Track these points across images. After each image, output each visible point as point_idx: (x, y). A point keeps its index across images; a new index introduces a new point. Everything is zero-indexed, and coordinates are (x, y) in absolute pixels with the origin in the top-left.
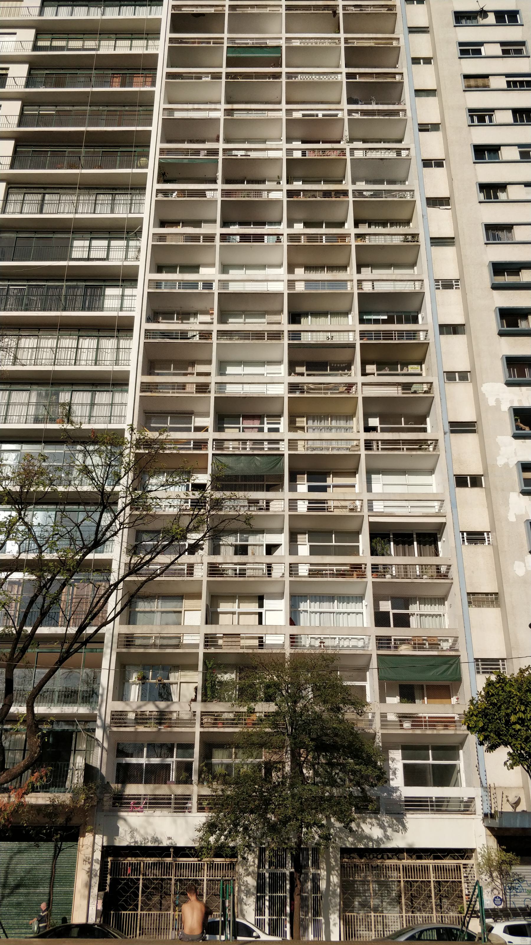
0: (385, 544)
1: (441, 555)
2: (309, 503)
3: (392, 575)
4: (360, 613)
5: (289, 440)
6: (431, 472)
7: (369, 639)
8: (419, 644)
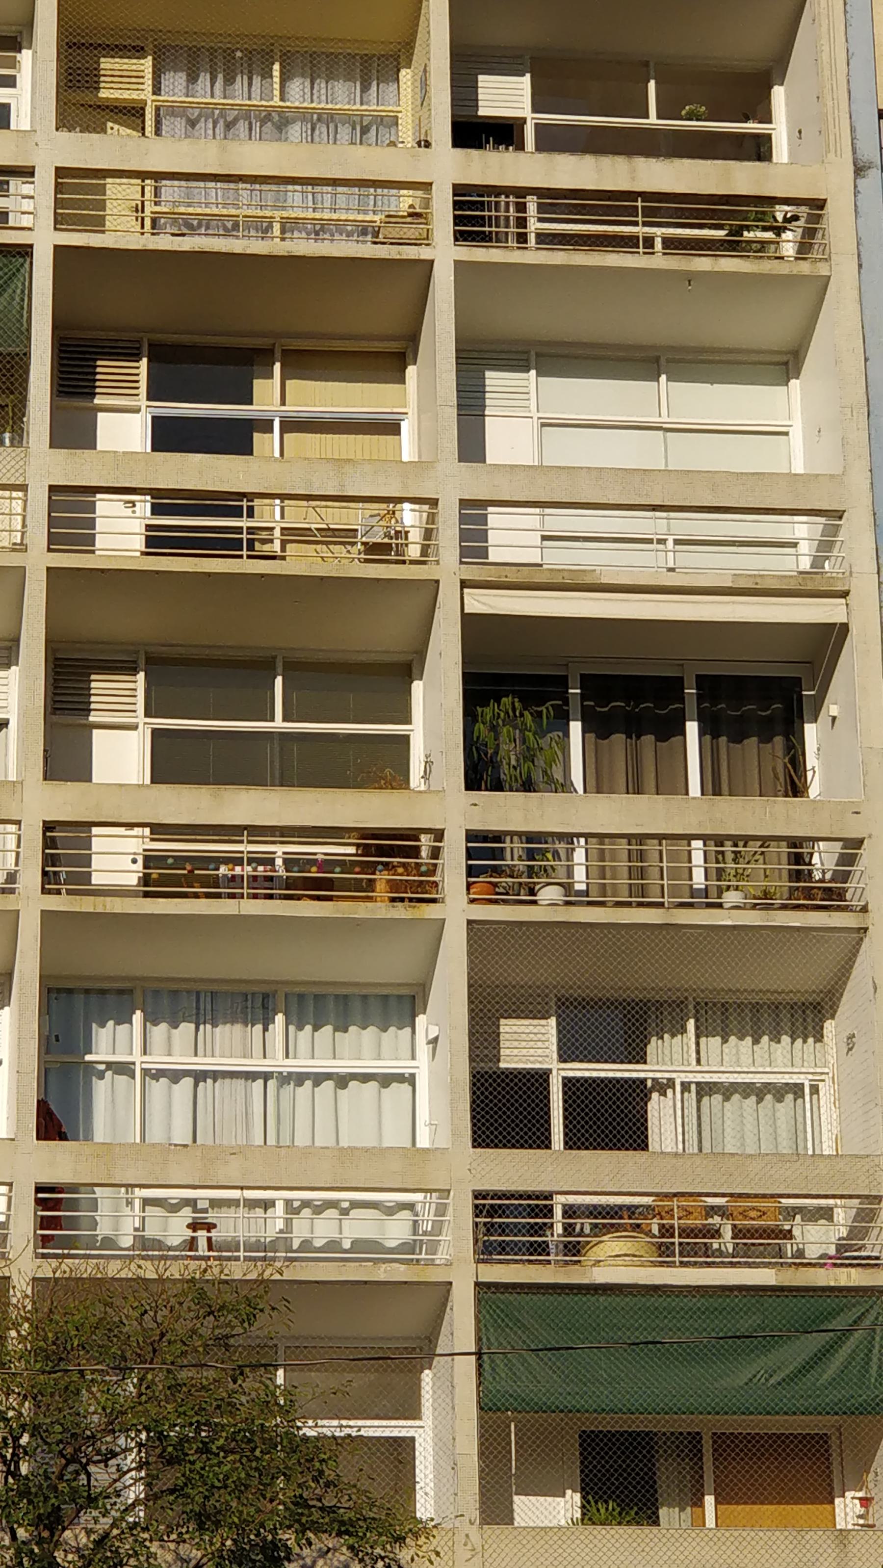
0: (541, 733)
1: (814, 791)
2: (156, 510)
3: (568, 888)
4: (400, 1078)
5: (60, 172)
6: (785, 364)
7: (441, 1210)
8: (686, 1232)
